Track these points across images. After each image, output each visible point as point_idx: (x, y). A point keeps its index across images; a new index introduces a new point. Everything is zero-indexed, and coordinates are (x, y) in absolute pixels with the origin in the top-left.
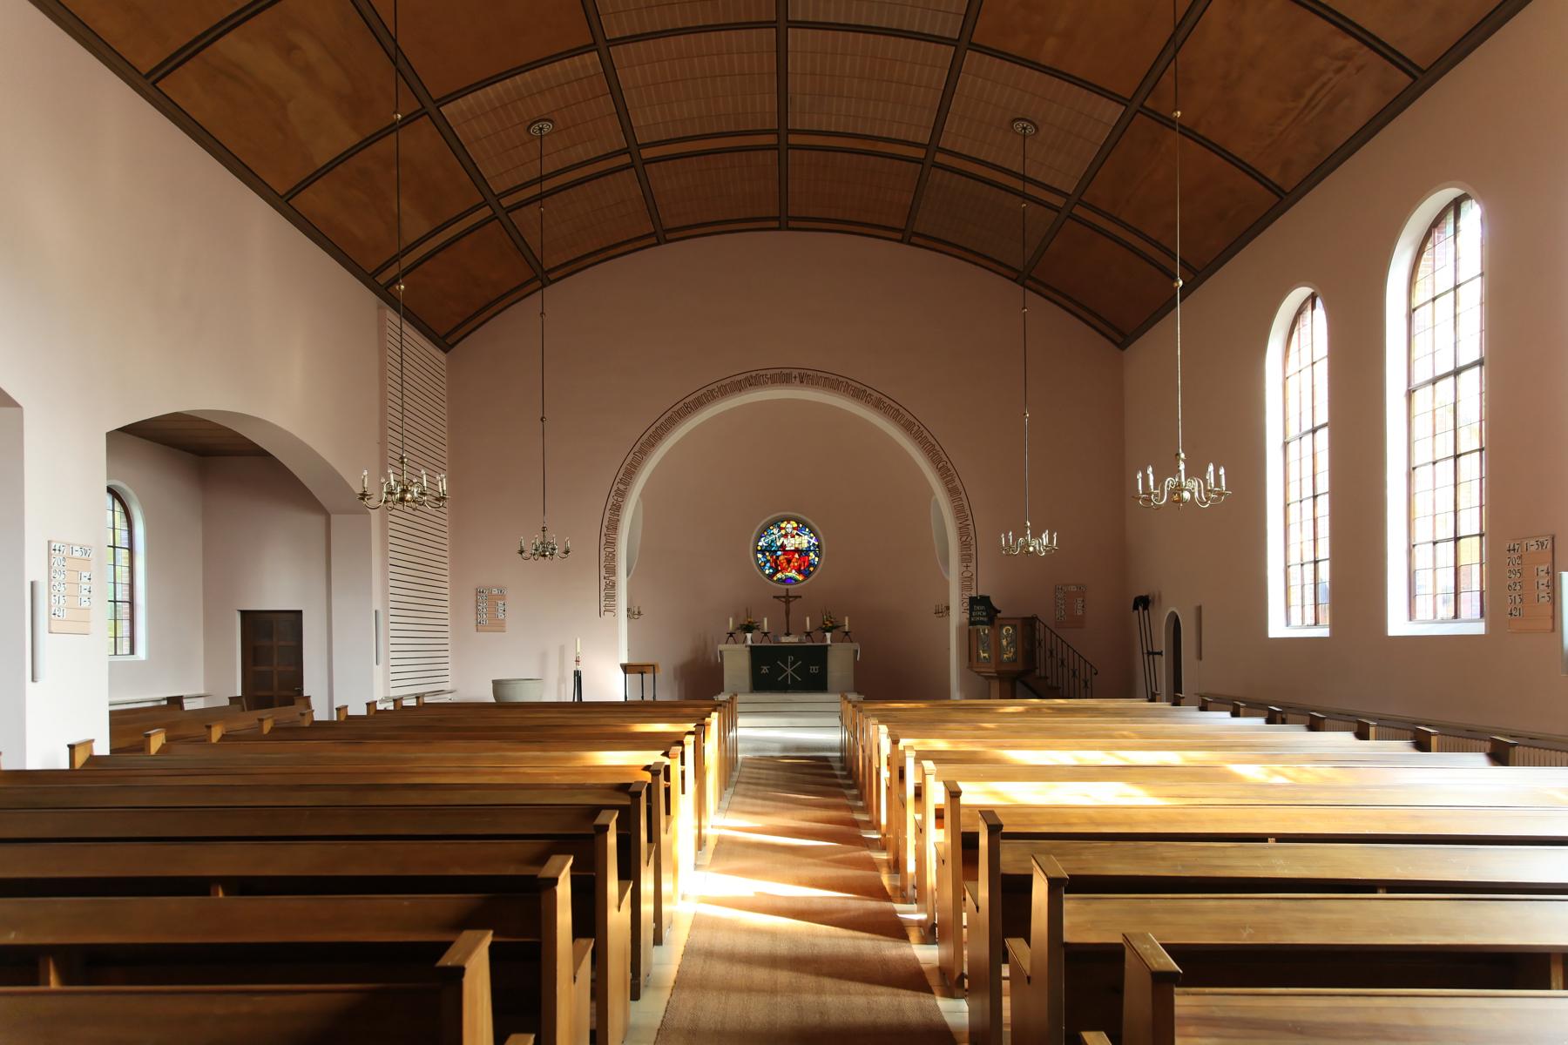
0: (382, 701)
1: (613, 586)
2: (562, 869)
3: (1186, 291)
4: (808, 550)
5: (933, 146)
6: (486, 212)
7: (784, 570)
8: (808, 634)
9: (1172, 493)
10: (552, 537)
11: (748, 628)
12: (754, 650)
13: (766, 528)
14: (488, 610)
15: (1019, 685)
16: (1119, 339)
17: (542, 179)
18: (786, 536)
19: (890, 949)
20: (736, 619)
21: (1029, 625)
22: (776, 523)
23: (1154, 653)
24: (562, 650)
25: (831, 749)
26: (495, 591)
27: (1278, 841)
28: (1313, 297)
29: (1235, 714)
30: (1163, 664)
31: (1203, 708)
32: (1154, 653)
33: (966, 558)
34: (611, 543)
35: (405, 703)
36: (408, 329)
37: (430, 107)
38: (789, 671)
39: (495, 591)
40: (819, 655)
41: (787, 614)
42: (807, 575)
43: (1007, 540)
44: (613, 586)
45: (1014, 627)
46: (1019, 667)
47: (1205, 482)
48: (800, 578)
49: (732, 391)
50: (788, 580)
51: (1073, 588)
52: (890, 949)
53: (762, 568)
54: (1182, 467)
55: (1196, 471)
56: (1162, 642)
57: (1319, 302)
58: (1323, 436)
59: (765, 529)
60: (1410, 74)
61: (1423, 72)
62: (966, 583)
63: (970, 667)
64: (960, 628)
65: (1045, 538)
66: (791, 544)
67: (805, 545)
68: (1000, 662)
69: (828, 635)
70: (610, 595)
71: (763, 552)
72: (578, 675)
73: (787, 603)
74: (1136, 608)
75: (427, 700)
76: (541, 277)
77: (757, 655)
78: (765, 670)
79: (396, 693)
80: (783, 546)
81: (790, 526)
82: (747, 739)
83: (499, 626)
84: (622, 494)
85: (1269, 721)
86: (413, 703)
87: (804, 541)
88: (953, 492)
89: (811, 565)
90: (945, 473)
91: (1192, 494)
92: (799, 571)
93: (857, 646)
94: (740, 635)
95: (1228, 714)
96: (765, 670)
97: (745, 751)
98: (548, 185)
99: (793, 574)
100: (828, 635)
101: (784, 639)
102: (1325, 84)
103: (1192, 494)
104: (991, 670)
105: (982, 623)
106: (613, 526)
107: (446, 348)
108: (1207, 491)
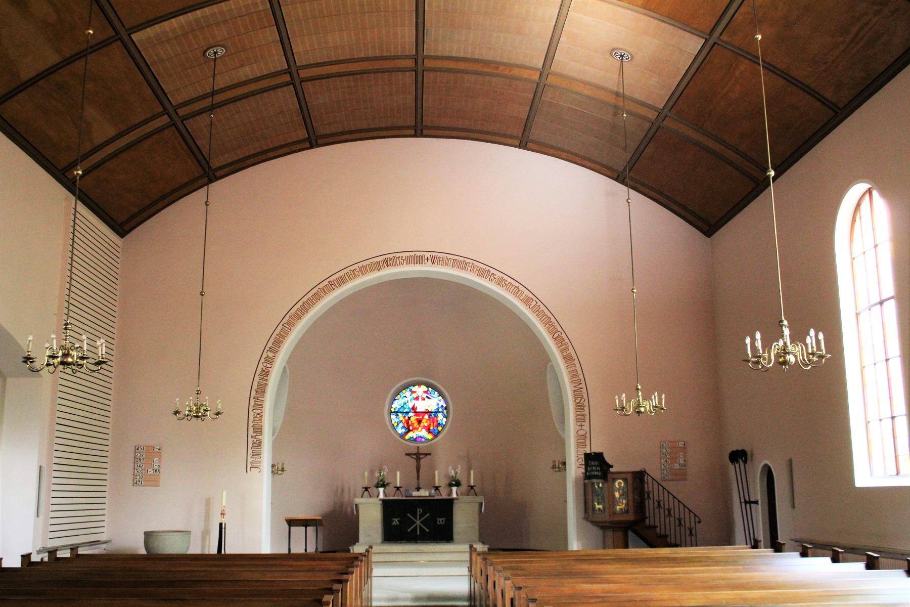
0: (39, 552)
1: (259, 444)
3: (774, 179)
4: (437, 412)
5: (545, 71)
6: (165, 119)
9: (778, 356)
10: (206, 400)
12: (386, 504)
13: (398, 393)
15: (630, 533)
17: (213, 93)
18: (417, 399)
20: (372, 472)
21: (639, 477)
23: (750, 502)
28: (870, 191)
29: (835, 560)
30: (759, 513)
31: (804, 554)
32: (750, 502)
33: (580, 418)
35: (60, 554)
36: (82, 209)
37: (124, 34)
40: (446, 507)
43: (621, 401)
44: (260, 445)
45: (625, 480)
46: (631, 517)
47: (806, 345)
48: (430, 437)
54: (787, 332)
55: (798, 337)
56: (758, 492)
57: (875, 193)
58: (891, 307)
60: (833, 110)
61: (839, 108)
62: (582, 440)
63: (586, 518)
64: (577, 481)
65: (655, 400)
66: (421, 406)
68: (614, 513)
69: (454, 489)
71: (396, 413)
73: (418, 459)
75: (81, 551)
76: (208, 174)
78: (396, 522)
79: (51, 544)
80: (414, 409)
81: (420, 390)
83: (153, 481)
85: (869, 566)
86: (66, 554)
87: (433, 403)
89: (439, 424)
91: (796, 357)
92: (429, 431)
93: (481, 499)
95: (828, 560)
96: (396, 522)
98: (219, 98)
99: (424, 433)
101: (415, 493)
102: (866, 24)
103: (796, 357)
105: (596, 477)
108: (808, 354)
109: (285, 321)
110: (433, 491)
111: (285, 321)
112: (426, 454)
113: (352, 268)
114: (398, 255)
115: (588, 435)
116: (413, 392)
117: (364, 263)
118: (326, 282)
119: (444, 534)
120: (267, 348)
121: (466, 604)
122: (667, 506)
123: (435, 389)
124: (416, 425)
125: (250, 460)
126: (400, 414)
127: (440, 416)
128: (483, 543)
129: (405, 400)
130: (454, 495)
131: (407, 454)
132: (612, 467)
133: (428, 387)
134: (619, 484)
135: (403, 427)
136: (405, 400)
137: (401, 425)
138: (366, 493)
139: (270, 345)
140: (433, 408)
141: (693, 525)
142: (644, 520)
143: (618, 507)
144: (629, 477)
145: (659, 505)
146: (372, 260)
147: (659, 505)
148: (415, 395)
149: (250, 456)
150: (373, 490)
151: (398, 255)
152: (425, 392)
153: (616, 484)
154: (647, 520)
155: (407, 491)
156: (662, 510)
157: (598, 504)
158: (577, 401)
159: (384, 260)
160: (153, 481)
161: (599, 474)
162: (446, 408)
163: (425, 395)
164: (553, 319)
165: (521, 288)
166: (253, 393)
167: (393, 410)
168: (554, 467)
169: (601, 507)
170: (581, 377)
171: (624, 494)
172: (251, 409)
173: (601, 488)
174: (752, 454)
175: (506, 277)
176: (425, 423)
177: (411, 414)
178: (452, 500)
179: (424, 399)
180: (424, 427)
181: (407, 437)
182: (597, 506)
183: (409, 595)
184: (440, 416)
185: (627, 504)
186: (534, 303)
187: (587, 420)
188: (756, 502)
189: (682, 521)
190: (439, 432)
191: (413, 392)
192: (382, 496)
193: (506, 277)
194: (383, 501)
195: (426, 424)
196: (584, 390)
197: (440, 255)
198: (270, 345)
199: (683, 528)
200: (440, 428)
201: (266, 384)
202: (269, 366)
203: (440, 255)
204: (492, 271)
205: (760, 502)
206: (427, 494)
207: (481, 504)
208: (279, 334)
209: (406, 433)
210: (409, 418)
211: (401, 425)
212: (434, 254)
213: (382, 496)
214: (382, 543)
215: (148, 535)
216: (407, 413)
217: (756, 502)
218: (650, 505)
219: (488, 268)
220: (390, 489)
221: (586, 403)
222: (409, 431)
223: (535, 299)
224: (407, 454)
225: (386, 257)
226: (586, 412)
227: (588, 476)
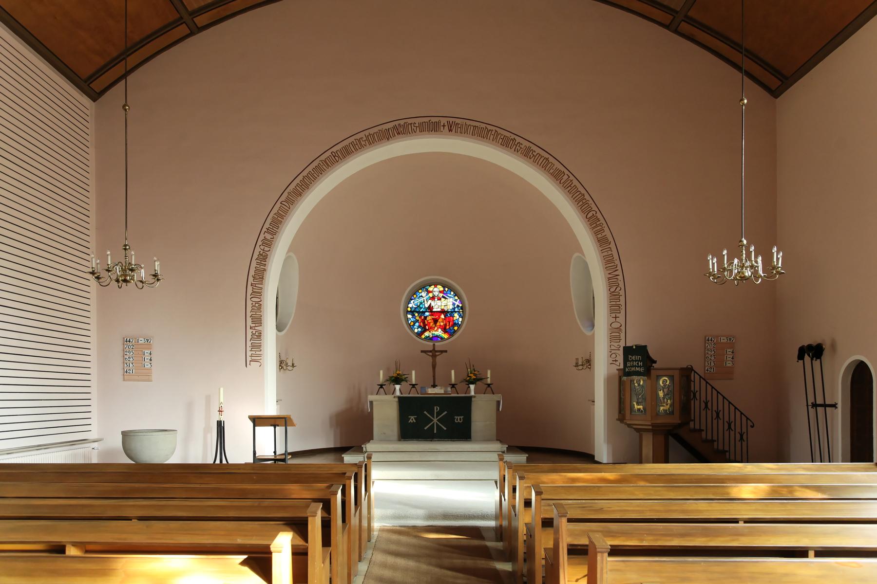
1: (259, 336)
2: (317, 510)
4: (453, 311)
7: (431, 328)
8: (453, 386)
11: (397, 380)
14: (134, 359)
16: (774, 83)
18: (433, 298)
19: (482, 563)
21: (686, 373)
22: (424, 287)
23: (825, 406)
24: (208, 399)
25: (483, 517)
26: (142, 341)
27: (745, 522)
32: (825, 406)
33: (614, 308)
34: (258, 293)
38: (435, 420)
39: (142, 341)
40: (464, 405)
41: (434, 367)
42: (451, 333)
45: (671, 378)
46: (676, 420)
48: (445, 336)
49: (380, 140)
50: (435, 338)
51: (724, 340)
52: (482, 563)
53: (411, 327)
56: (838, 391)
59: (414, 293)
62: (614, 334)
63: (622, 418)
64: (608, 380)
66: (437, 306)
67: (450, 307)
68: (657, 414)
69: (472, 387)
71: (412, 312)
72: (220, 426)
73: (434, 356)
74: (801, 357)
77: (405, 404)
78: (412, 419)
80: (430, 308)
81: (437, 290)
82: (388, 501)
83: (146, 376)
84: (268, 244)
87: (449, 303)
88: (602, 242)
89: (455, 324)
90: (595, 222)
92: (445, 330)
93: (498, 397)
94: (389, 387)
97: (383, 518)
99: (439, 333)
100: (472, 387)
101: (431, 391)
104: (645, 422)
105: (638, 374)
106: (260, 276)
107: (95, 96)
109: (283, 198)
110: (449, 389)
111: (283, 198)
112: (442, 352)
113: (358, 137)
114: (409, 121)
115: (623, 328)
116: (429, 292)
117: (372, 131)
118: (328, 153)
119: (460, 432)
120: (264, 229)
121: (492, 523)
122: (715, 408)
123: (451, 289)
125: (249, 353)
127: (456, 315)
128: (501, 442)
129: (421, 299)
130: (473, 393)
131: (422, 351)
132: (655, 362)
133: (444, 287)
135: (419, 327)
136: (421, 299)
137: (417, 324)
138: (382, 390)
139: (267, 225)
141: (744, 430)
142: (688, 423)
143: (662, 408)
144: (677, 374)
145: (706, 406)
146: (380, 128)
147: (706, 406)
148: (431, 295)
149: (249, 349)
151: (409, 121)
152: (440, 292)
153: (661, 383)
154: (692, 424)
156: (709, 413)
157: (638, 404)
158: (612, 290)
159: (395, 127)
160: (146, 376)
161: (642, 370)
162: (462, 308)
164: (587, 197)
165: (551, 159)
166: (251, 279)
168: (577, 365)
169: (641, 407)
170: (618, 262)
171: (669, 394)
172: (249, 297)
173: (642, 386)
174: (833, 346)
175: (534, 148)
177: (427, 314)
179: (439, 299)
180: (440, 327)
181: (423, 337)
182: (636, 407)
183: (421, 512)
184: (456, 315)
185: (672, 405)
186: (566, 177)
187: (623, 312)
188: (834, 406)
189: (733, 425)
190: (455, 331)
191: (429, 292)
192: (398, 393)
193: (534, 148)
194: (399, 398)
196: (620, 278)
197: (458, 121)
198: (267, 225)
199: (732, 433)
200: (456, 328)
201: (265, 270)
202: (267, 249)
203: (458, 121)
204: (518, 139)
205: (839, 406)
207: (498, 402)
208: (277, 214)
210: (426, 318)
211: (417, 324)
212: (451, 120)
213: (398, 393)
214: (399, 440)
215: (125, 435)
217: (834, 406)
218: (695, 405)
219: (513, 136)
221: (622, 292)
222: (425, 330)
223: (566, 172)
224: (422, 351)
225: (397, 123)
226: (622, 302)
227: (626, 372)
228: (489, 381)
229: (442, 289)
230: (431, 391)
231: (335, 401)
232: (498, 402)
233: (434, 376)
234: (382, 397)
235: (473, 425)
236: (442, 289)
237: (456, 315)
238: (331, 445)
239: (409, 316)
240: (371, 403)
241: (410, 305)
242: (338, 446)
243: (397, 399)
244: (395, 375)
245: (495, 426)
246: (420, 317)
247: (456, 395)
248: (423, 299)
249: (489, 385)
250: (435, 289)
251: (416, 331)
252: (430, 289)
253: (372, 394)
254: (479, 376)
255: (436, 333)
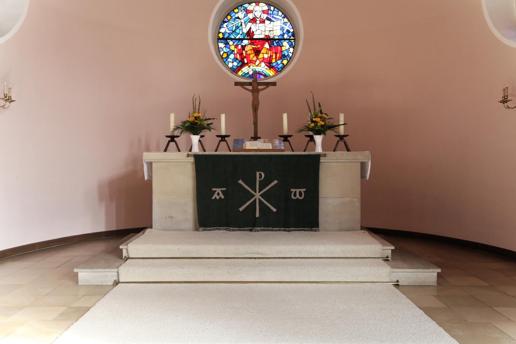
4: (281, 39)
8: (285, 138)
11: (194, 126)
12: (201, 162)
18: (253, 20)
38: (258, 195)
40: (306, 170)
41: (255, 108)
53: (224, 60)
69: (318, 139)
70: (211, 124)
71: (225, 40)
73: (255, 92)
78: (218, 193)
80: (250, 34)
81: (258, 9)
87: (276, 27)
89: (283, 57)
92: (270, 65)
93: (365, 156)
96: (218, 193)
99: (263, 68)
100: (318, 139)
101: (249, 145)
110: (277, 142)
112: (268, 84)
116: (248, 12)
123: (279, 8)
124: (252, 57)
126: (231, 43)
129: (238, 22)
130: (319, 150)
133: (269, 5)
134: (261, 176)
135: (235, 59)
136: (238, 22)
137: (232, 56)
138: (172, 144)
140: (277, 33)
150: (181, 140)
152: (264, 12)
155: (236, 141)
163: (265, 16)
167: (221, 36)
176: (265, 55)
177: (245, 42)
178: (317, 158)
179: (263, 22)
181: (240, 73)
191: (248, 12)
194: (196, 156)
195: (266, 56)
200: (285, 62)
206: (269, 146)
207: (363, 165)
209: (239, 68)
210: (243, 47)
211: (232, 56)
213: (196, 149)
214: (197, 230)
216: (241, 40)
220: (210, 136)
222: (243, 65)
228: (342, 130)
229: (266, 8)
230: (249, 145)
231: (110, 164)
232: (363, 165)
233: (255, 124)
234: (172, 155)
235: (321, 201)
236: (266, 8)
237: (285, 43)
238: (101, 228)
239: (221, 45)
240: (150, 164)
241: (223, 30)
242: (114, 228)
243: (192, 159)
244: (192, 119)
245: (358, 205)
246: (236, 46)
247: (290, 153)
248: (241, 22)
249: (341, 137)
250: (257, 8)
251: (230, 65)
252: (250, 7)
253: (148, 150)
254: (329, 122)
255: (258, 69)
